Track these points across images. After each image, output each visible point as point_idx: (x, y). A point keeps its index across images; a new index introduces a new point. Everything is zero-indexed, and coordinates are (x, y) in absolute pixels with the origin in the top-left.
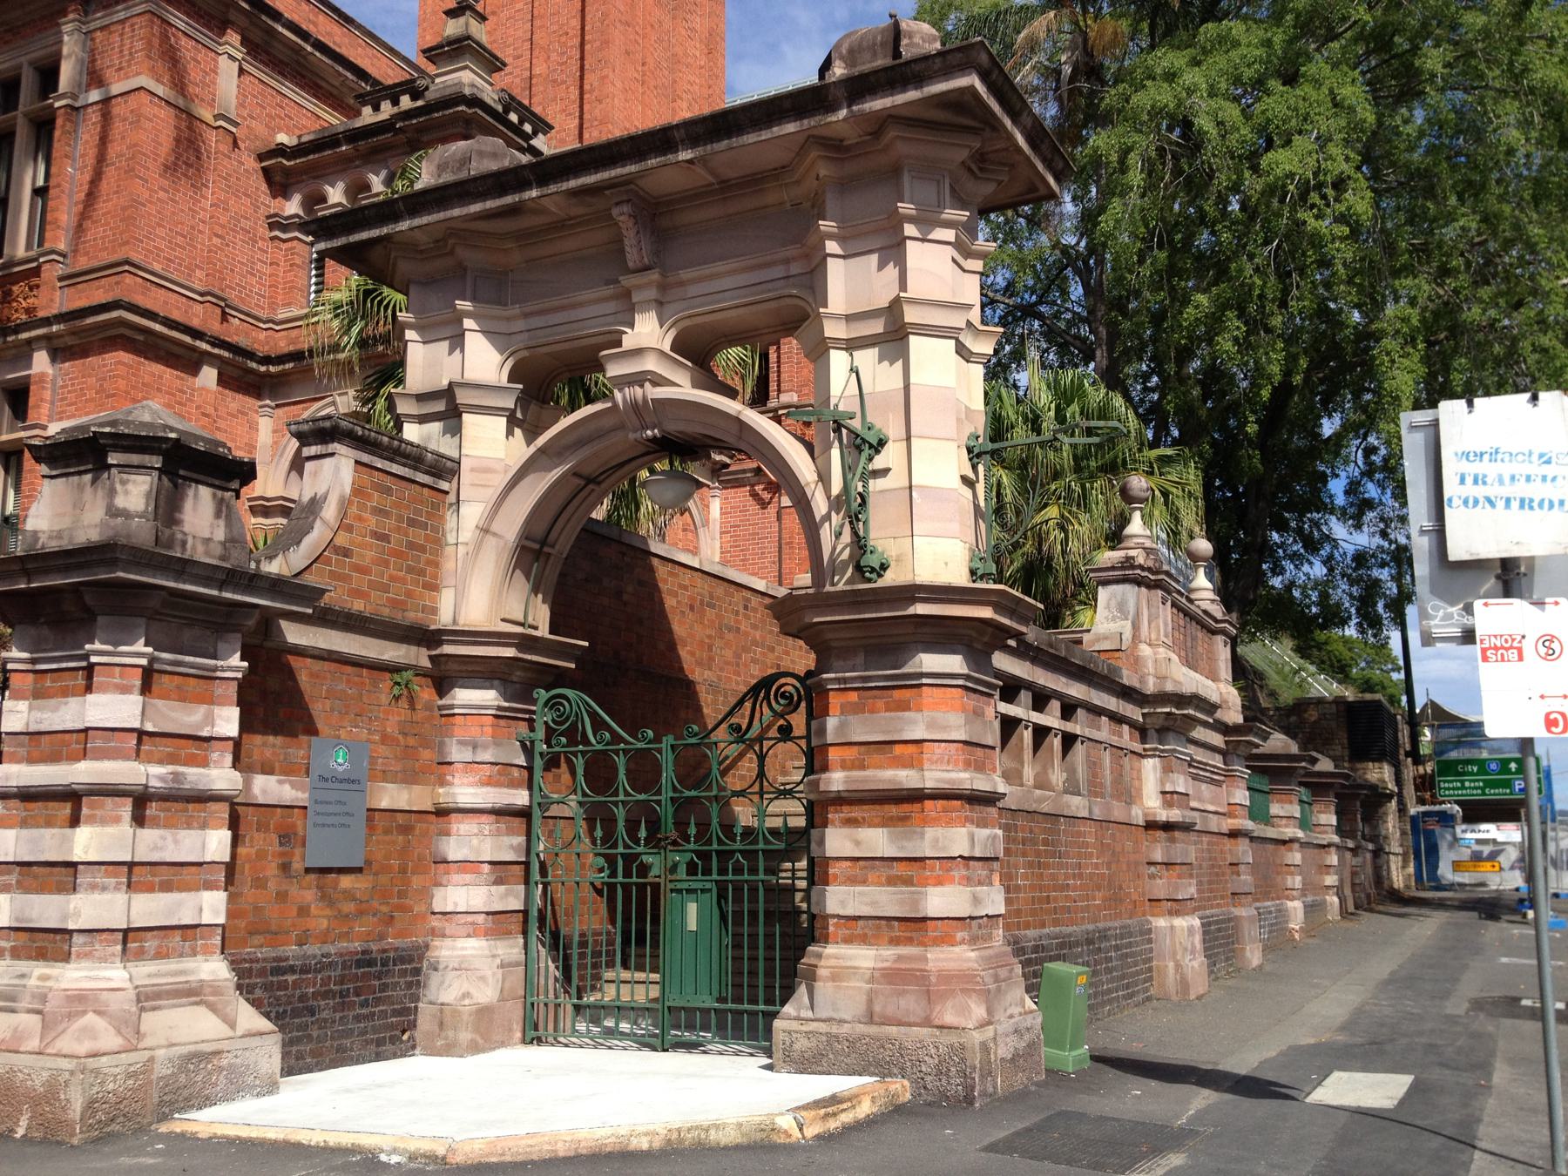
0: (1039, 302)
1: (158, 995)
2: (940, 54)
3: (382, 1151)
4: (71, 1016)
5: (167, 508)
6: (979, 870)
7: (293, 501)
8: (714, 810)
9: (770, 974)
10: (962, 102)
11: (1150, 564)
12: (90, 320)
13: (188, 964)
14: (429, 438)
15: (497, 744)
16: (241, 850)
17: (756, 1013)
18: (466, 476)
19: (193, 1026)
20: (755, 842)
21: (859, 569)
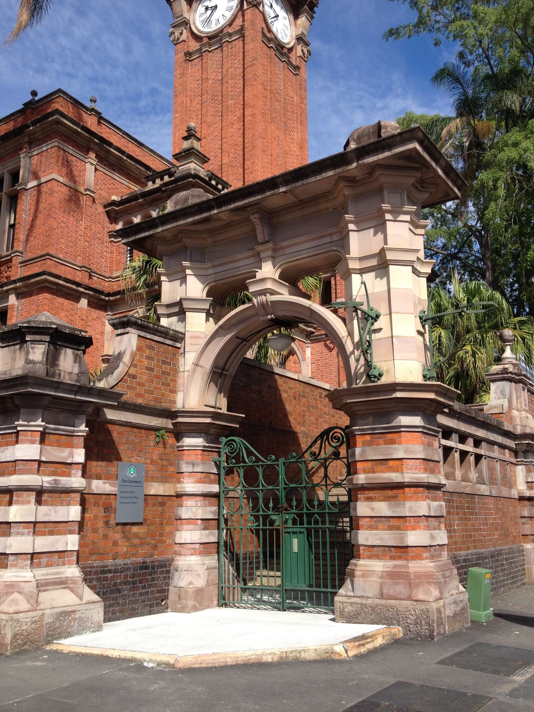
0: (460, 251)
1: (47, 584)
2: (399, 134)
3: (145, 661)
4: (7, 594)
5: (52, 359)
6: (434, 522)
7: (110, 356)
8: (304, 493)
9: (333, 573)
10: (411, 156)
11: (516, 371)
12: (32, 280)
13: (61, 569)
14: (171, 324)
15: (203, 463)
16: (86, 515)
17: (327, 592)
18: (188, 340)
19: (63, 599)
20: (324, 509)
21: (368, 376)
